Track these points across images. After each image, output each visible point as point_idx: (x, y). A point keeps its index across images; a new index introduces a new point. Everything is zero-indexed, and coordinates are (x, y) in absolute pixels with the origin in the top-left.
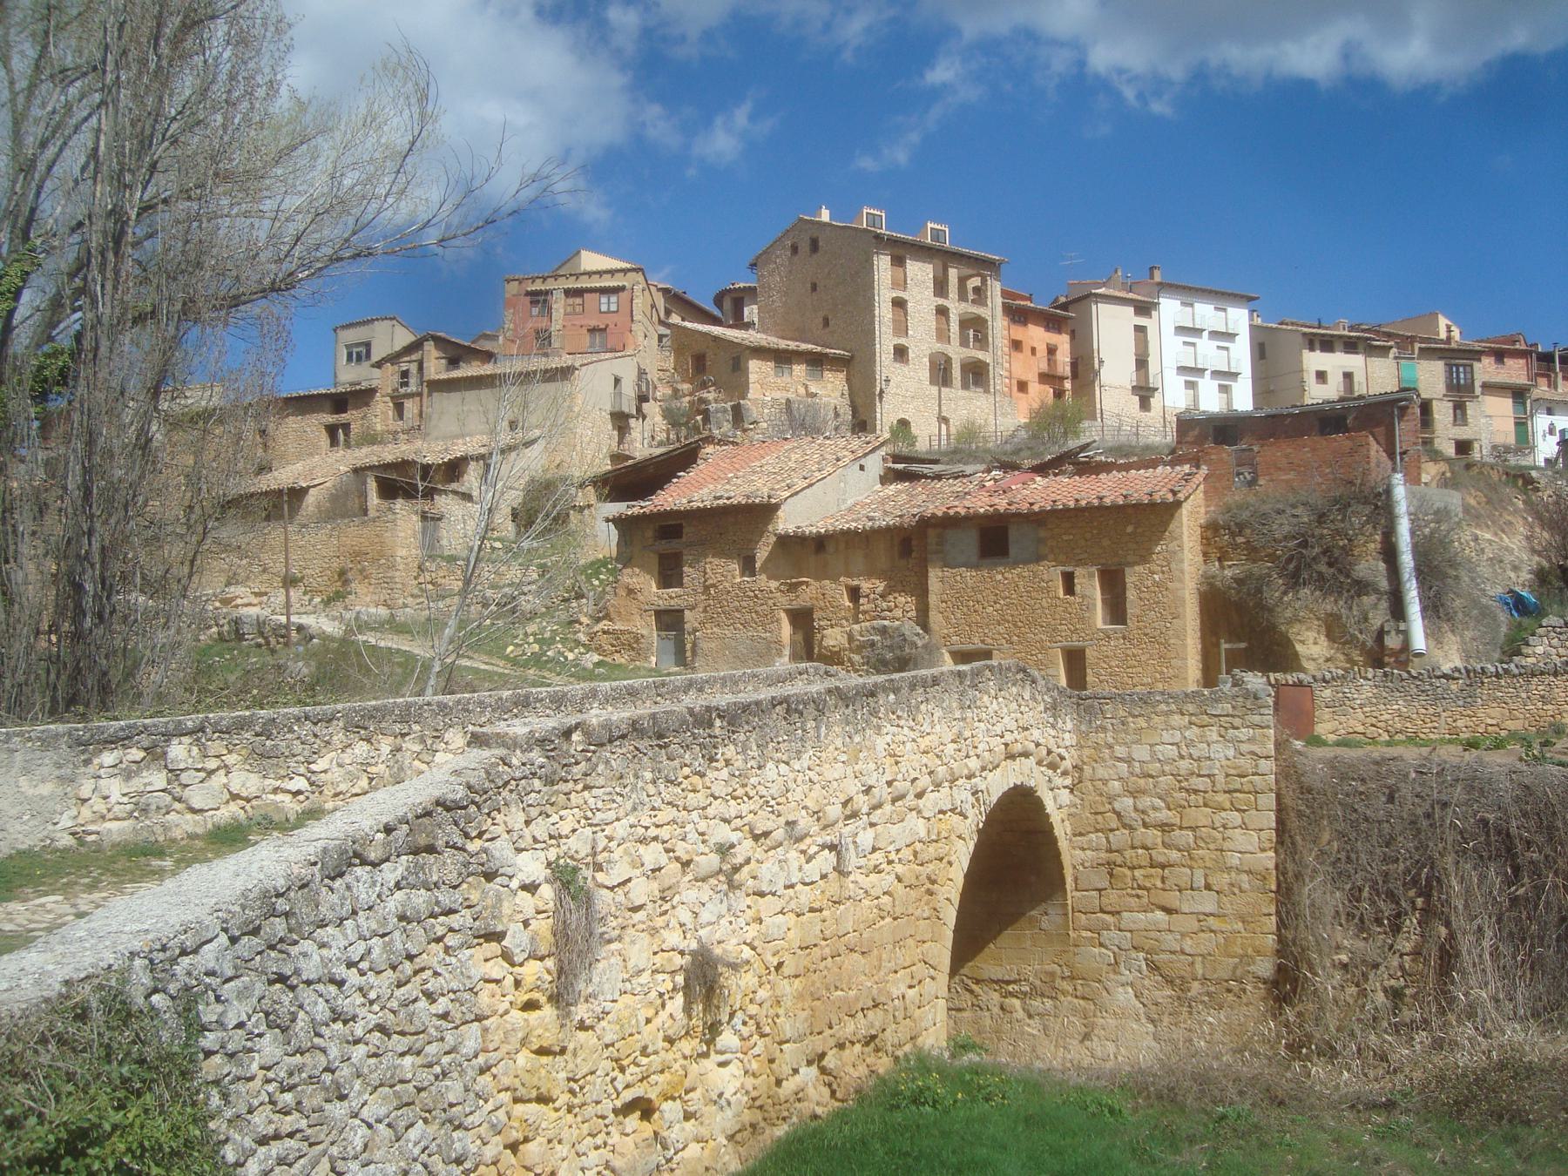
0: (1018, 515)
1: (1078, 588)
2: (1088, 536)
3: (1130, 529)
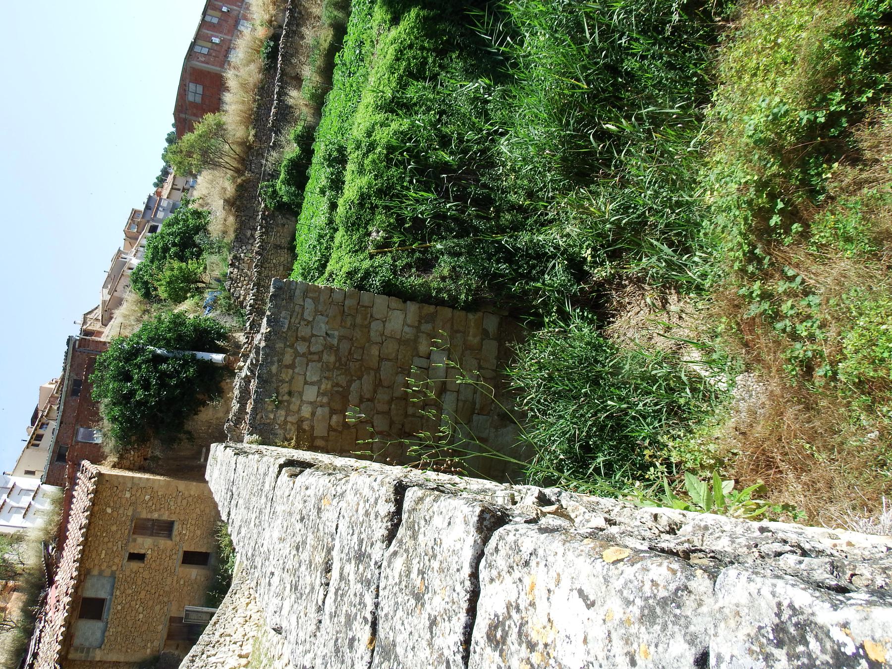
0: (76, 588)
1: (142, 552)
2: (106, 539)
3: (109, 510)
